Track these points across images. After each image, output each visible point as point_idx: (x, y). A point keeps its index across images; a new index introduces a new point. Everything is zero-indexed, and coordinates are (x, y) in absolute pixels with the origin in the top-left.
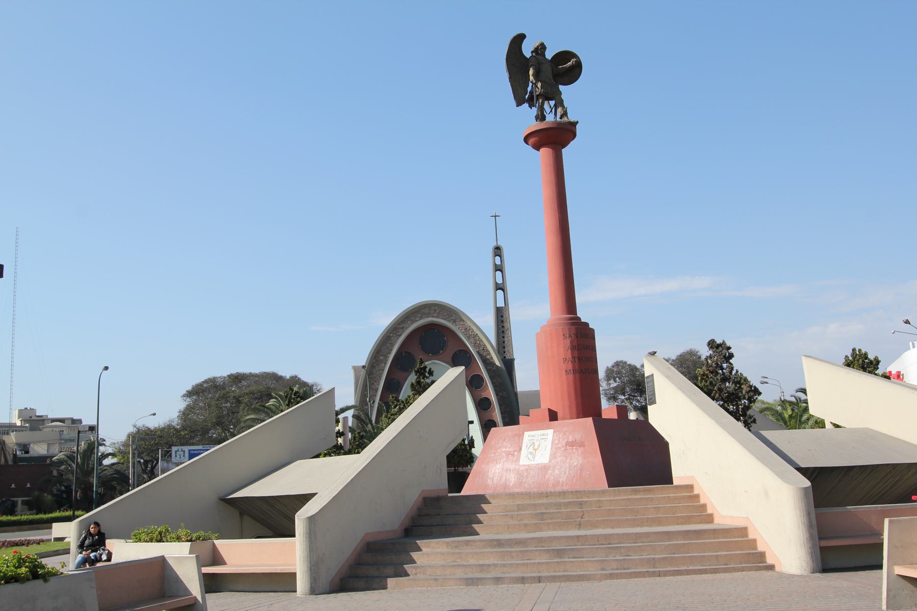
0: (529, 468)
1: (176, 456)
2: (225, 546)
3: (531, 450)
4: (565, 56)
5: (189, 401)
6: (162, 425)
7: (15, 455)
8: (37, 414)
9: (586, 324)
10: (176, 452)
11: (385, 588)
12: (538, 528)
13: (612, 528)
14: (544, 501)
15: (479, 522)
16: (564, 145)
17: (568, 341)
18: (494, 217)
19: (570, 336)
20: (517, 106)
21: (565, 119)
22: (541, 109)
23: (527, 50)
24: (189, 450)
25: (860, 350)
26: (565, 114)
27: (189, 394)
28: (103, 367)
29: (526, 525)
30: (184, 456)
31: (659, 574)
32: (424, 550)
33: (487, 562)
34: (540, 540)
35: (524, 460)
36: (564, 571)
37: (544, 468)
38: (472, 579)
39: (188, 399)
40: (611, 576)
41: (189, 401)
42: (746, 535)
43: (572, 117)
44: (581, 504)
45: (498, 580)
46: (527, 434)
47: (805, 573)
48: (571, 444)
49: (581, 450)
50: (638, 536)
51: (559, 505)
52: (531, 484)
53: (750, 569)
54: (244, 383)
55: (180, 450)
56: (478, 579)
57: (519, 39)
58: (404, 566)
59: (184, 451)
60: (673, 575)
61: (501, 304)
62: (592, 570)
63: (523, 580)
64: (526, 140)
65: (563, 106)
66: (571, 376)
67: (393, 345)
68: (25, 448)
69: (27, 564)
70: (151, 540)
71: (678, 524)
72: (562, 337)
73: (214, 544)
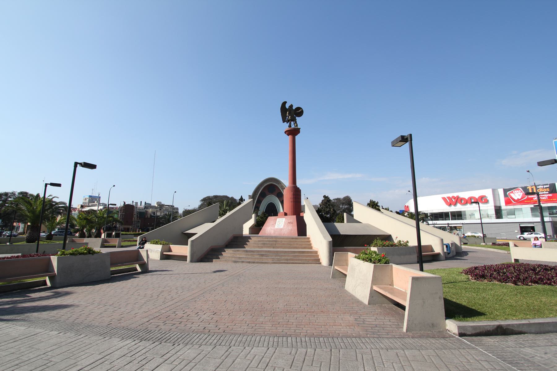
0: (277, 229)
2: (172, 247)
3: (278, 224)
4: (298, 108)
5: (202, 202)
6: (192, 209)
7: (151, 215)
8: (162, 203)
9: (299, 188)
11: (212, 262)
12: (262, 247)
13: (283, 249)
14: (267, 240)
15: (247, 245)
16: (296, 135)
17: (292, 193)
19: (293, 191)
20: (283, 123)
21: (297, 127)
22: (290, 124)
23: (287, 106)
25: (372, 200)
26: (297, 126)
27: (202, 200)
28: (174, 192)
29: (259, 246)
31: (288, 263)
32: (226, 252)
33: (242, 256)
34: (258, 251)
35: (276, 227)
36: (262, 261)
37: (281, 229)
38: (236, 261)
39: (202, 202)
40: (274, 263)
41: (202, 202)
42: (317, 254)
43: (299, 127)
44: (276, 241)
45: (243, 262)
46: (278, 219)
47: (327, 266)
48: (289, 223)
49: (292, 225)
50: (286, 252)
51: (270, 241)
52: (277, 234)
53: (314, 263)
54: (218, 198)
56: (238, 261)
57: (285, 103)
58: (219, 256)
60: (291, 264)
62: (270, 261)
63: (249, 262)
64: (285, 132)
65: (297, 123)
66: (292, 203)
67: (260, 190)
68: (154, 213)
70: (154, 244)
71: (302, 249)
72: (290, 191)
73: (170, 246)
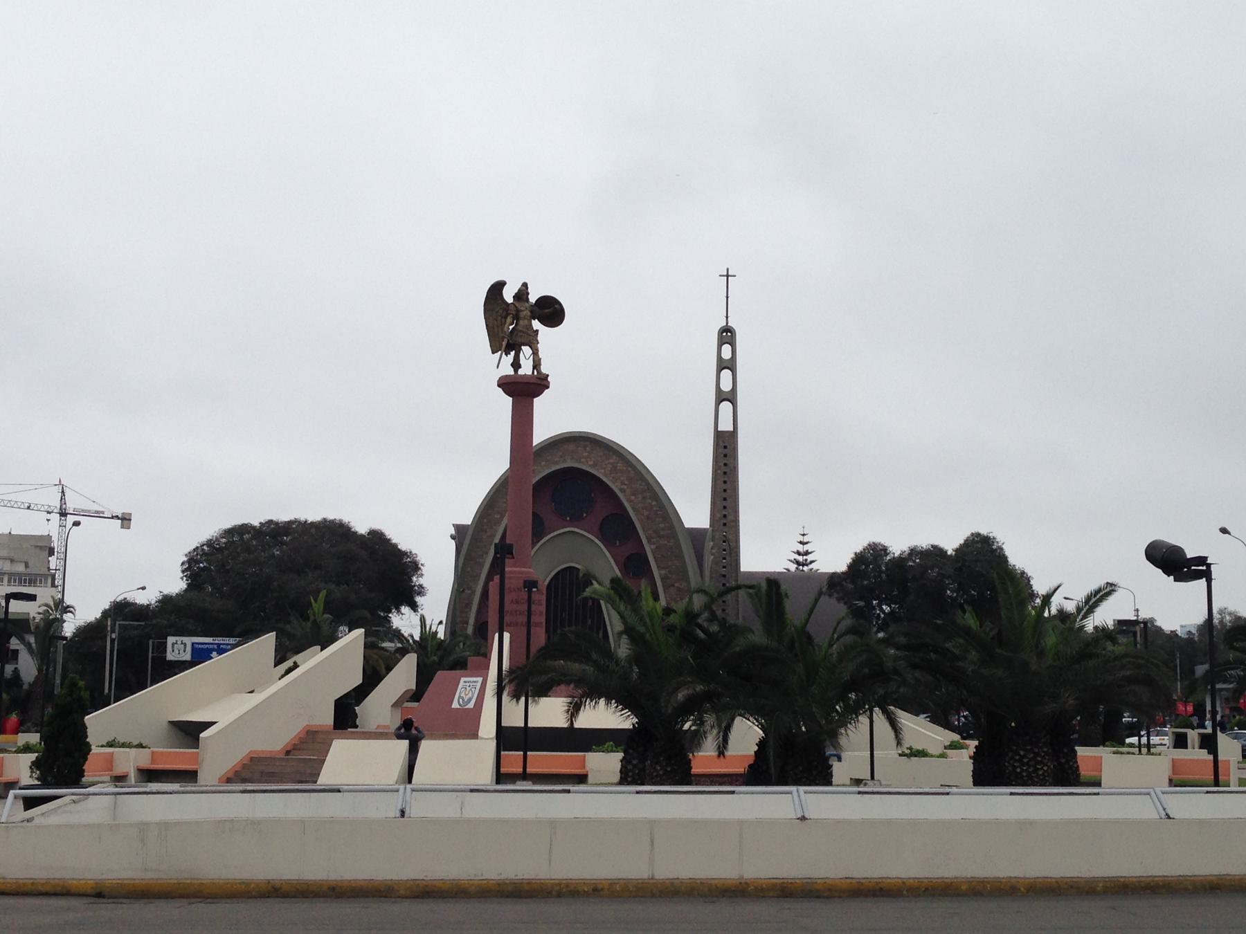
1: (173, 651)
10: (173, 644)
18: (725, 274)
24: (193, 644)
30: (184, 651)
55: (179, 642)
59: (185, 645)
61: (726, 425)
69: (1043, 740)
